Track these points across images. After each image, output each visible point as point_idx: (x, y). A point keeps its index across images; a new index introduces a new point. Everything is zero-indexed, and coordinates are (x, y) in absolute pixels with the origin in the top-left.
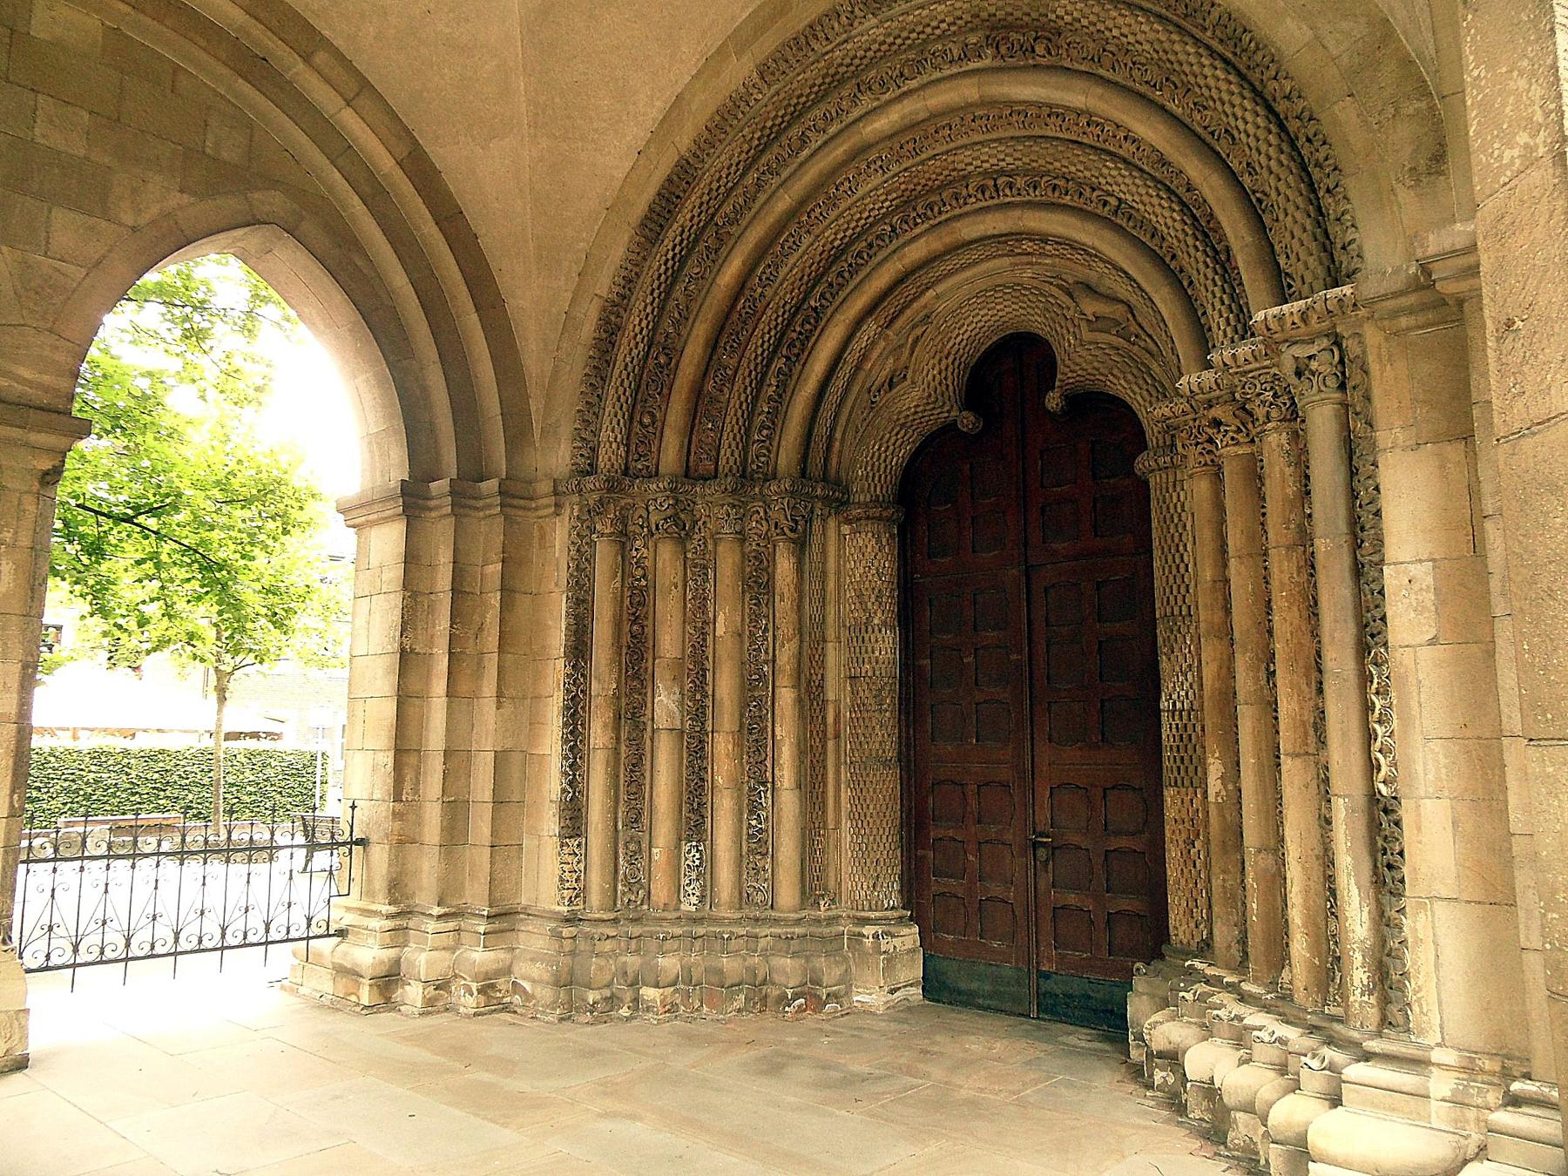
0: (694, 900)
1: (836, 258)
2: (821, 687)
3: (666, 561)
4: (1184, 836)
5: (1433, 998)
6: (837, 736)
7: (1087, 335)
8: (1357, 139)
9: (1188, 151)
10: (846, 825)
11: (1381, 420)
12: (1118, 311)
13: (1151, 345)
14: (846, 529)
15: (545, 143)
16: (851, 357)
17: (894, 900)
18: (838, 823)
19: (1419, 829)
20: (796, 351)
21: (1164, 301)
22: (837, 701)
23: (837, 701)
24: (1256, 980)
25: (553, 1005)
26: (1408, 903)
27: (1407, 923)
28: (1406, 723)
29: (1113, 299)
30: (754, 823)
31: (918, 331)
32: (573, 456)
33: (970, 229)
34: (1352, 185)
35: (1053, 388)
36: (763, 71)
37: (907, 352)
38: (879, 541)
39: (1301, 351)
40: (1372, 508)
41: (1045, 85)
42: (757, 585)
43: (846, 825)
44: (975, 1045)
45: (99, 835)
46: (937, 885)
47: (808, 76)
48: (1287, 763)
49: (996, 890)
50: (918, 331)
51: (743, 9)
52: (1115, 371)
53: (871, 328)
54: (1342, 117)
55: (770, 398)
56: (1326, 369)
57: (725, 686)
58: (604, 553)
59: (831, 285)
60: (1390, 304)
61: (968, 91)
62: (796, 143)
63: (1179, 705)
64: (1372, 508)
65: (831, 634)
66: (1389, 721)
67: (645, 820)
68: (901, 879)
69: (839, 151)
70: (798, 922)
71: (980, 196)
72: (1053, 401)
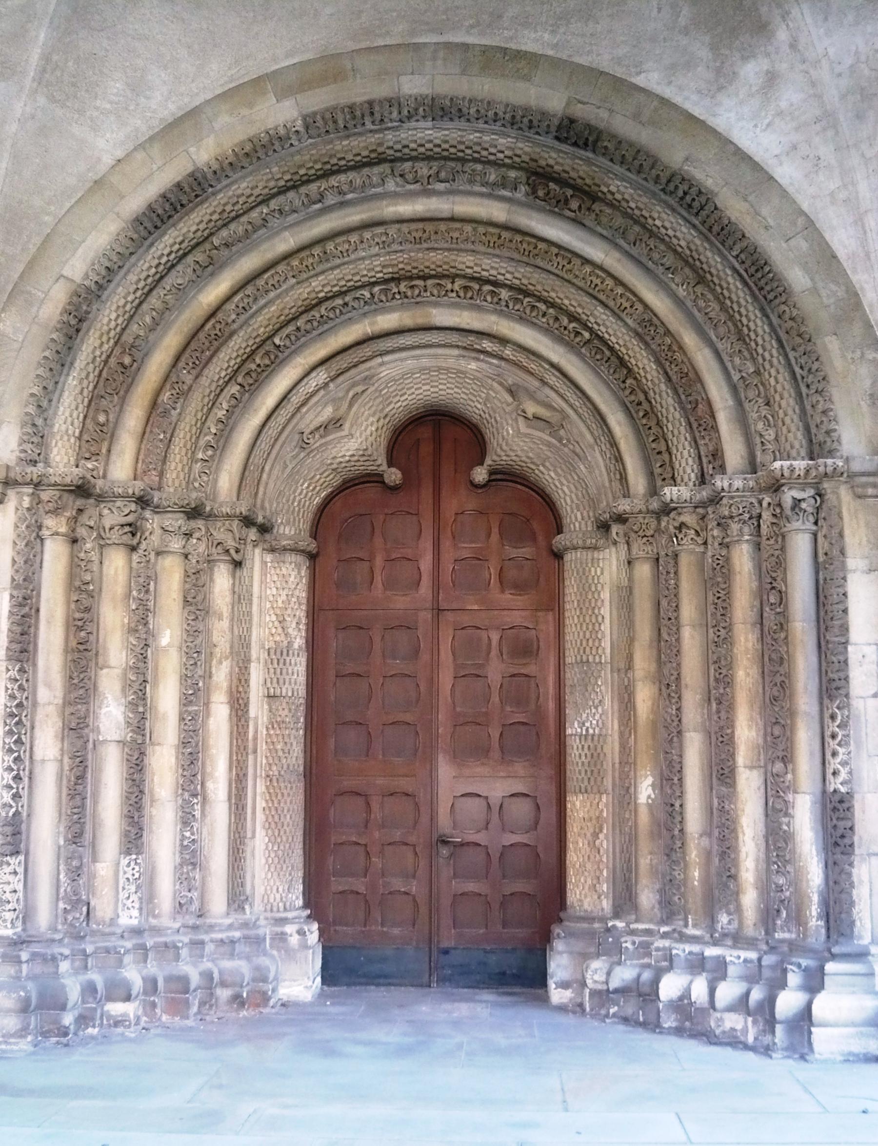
0: (135, 913)
1: (314, 307)
2: (246, 705)
3: (116, 566)
4: (592, 830)
5: (868, 914)
6: (255, 751)
7: (523, 428)
8: (838, 363)
9: (688, 325)
10: (260, 833)
11: (849, 552)
12: (554, 417)
13: (578, 450)
14: (269, 558)
15: (42, 100)
16: (295, 400)
17: (300, 902)
18: (254, 832)
19: (864, 812)
20: (251, 381)
21: (619, 423)
22: (256, 718)
23: (256, 718)
24: (695, 926)
25: (22, 1032)
26: (856, 860)
27: (855, 871)
28: (858, 746)
29: (549, 406)
30: (188, 834)
31: (359, 389)
32: (22, 442)
33: (442, 316)
34: (836, 393)
35: (482, 464)
36: (309, 122)
37: (345, 405)
38: (299, 573)
39: (799, 495)
40: (841, 607)
41: (568, 232)
42: (196, 604)
43: (260, 833)
44: (462, 1009)
45: (785, 820)
46: (338, 884)
47: (359, 145)
48: (258, 780)
49: (397, 884)
50: (359, 389)
51: (288, 56)
52: (547, 464)
53: (321, 376)
54: (830, 346)
55: (220, 421)
56: (810, 510)
57: (167, 698)
58: (54, 557)
59: (298, 329)
60: (864, 479)
61: (497, 211)
62: (315, 196)
63: (591, 731)
64: (841, 607)
65: (254, 654)
66: (847, 744)
67: (88, 836)
68: (304, 883)
69: (354, 216)
70: (230, 927)
71: (462, 294)
72: (480, 474)
